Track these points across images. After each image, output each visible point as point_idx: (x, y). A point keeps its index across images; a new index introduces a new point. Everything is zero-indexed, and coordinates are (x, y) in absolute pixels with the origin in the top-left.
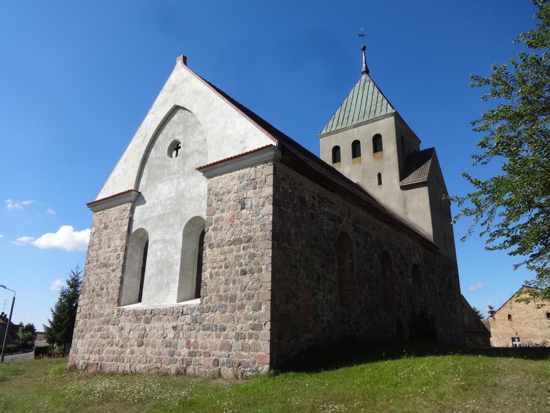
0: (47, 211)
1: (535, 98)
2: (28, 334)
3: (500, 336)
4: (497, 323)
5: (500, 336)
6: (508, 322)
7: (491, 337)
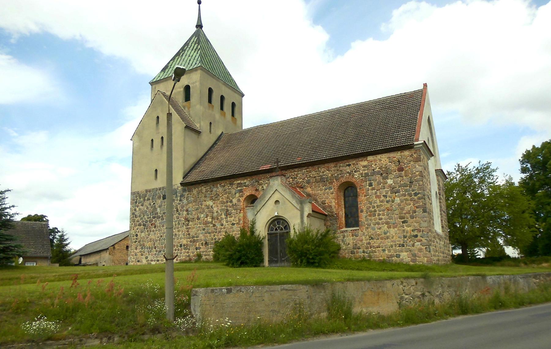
0: (536, 195)
1: (287, 240)
2: (319, 257)
3: (116, 262)
4: (115, 252)
5: (116, 262)
6: (126, 251)
7: (60, 265)
